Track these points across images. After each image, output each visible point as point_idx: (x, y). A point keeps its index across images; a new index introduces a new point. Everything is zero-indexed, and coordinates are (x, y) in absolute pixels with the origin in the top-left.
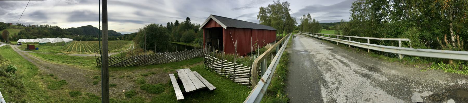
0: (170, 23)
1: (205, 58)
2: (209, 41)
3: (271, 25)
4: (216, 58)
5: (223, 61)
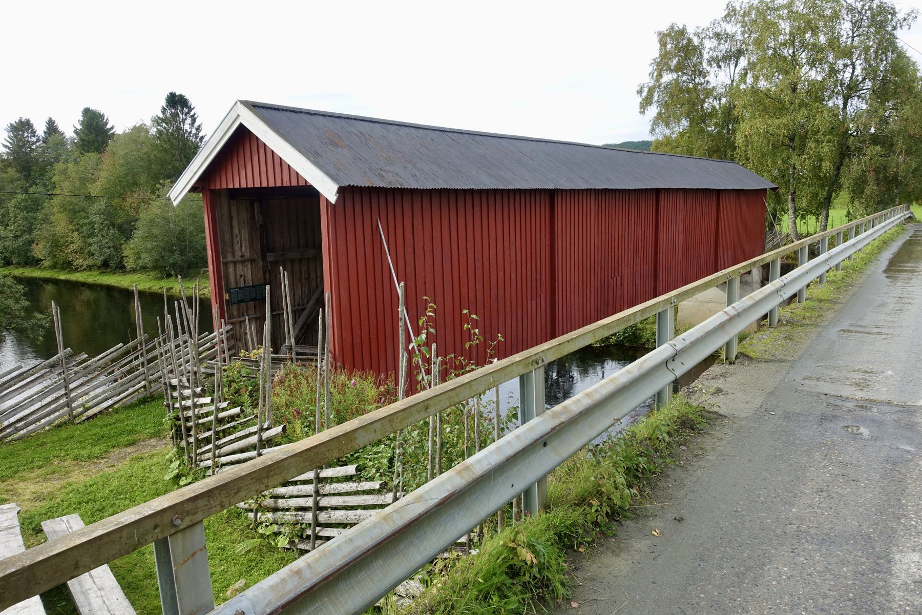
0: (40, 129)
5: (262, 430)
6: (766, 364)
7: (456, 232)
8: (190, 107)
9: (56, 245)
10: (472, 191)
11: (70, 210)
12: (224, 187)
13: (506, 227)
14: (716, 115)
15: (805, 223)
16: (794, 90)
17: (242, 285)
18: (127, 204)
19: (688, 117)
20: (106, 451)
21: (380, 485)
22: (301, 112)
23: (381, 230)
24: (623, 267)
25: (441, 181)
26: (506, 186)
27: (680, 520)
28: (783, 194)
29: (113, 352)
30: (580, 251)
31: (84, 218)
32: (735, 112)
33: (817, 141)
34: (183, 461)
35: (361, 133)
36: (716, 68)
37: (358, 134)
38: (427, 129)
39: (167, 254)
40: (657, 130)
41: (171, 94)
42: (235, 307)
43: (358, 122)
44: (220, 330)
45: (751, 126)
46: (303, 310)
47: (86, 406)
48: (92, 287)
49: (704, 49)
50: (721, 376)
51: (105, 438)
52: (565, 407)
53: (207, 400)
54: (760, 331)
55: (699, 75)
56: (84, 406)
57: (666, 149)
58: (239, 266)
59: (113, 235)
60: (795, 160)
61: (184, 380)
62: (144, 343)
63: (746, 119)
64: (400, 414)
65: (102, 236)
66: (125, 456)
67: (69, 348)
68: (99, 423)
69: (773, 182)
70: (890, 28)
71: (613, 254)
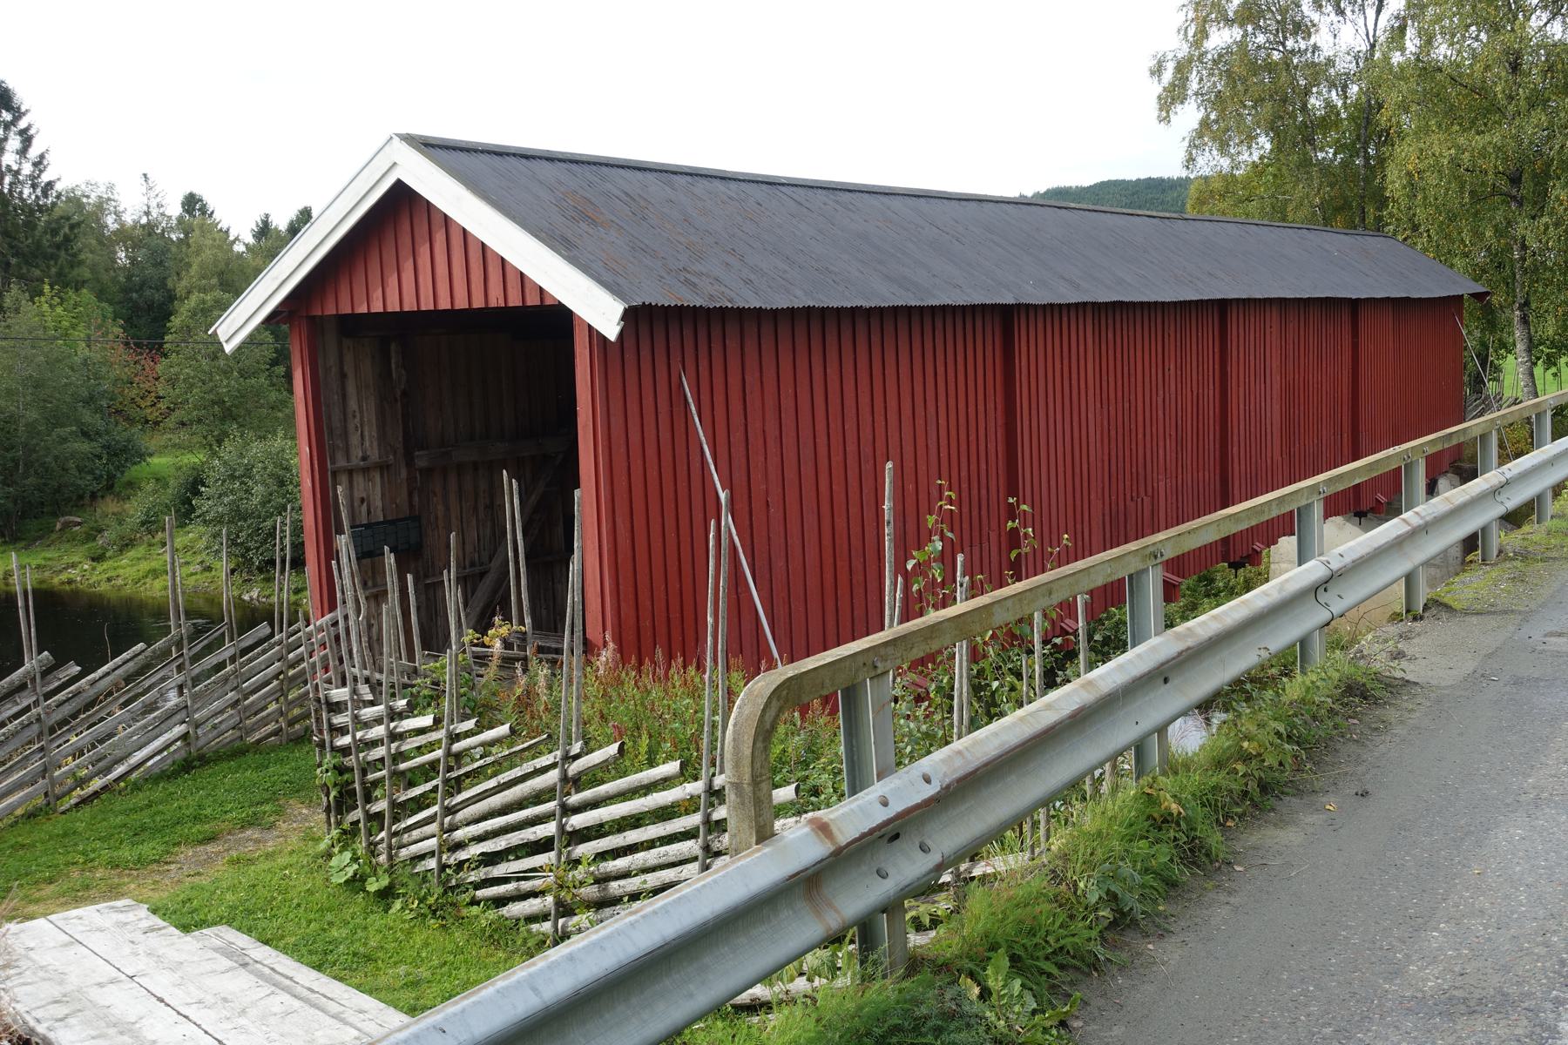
1: (345, 740)
3: (1382, 202)
4: (480, 728)
5: (569, 758)
6: (1479, 617)
8: (19, 108)
13: (918, 388)
14: (1339, 121)
15: (1555, 375)
16: (1515, 67)
17: (365, 522)
19: (1272, 129)
24: (1155, 475)
25: (799, 293)
26: (922, 300)
27: (1365, 794)
28: (1501, 307)
32: (1383, 119)
35: (627, 194)
36: (1333, 15)
38: (744, 181)
45: (1421, 150)
46: (482, 575)
50: (1401, 637)
52: (1189, 629)
53: (427, 721)
54: (1464, 571)
55: (1295, 33)
56: (74, 774)
57: (1222, 206)
58: (359, 480)
60: (1523, 228)
62: (185, 642)
63: (1408, 135)
64: (1028, 594)
67: (46, 653)
69: (1476, 279)
71: (1134, 447)
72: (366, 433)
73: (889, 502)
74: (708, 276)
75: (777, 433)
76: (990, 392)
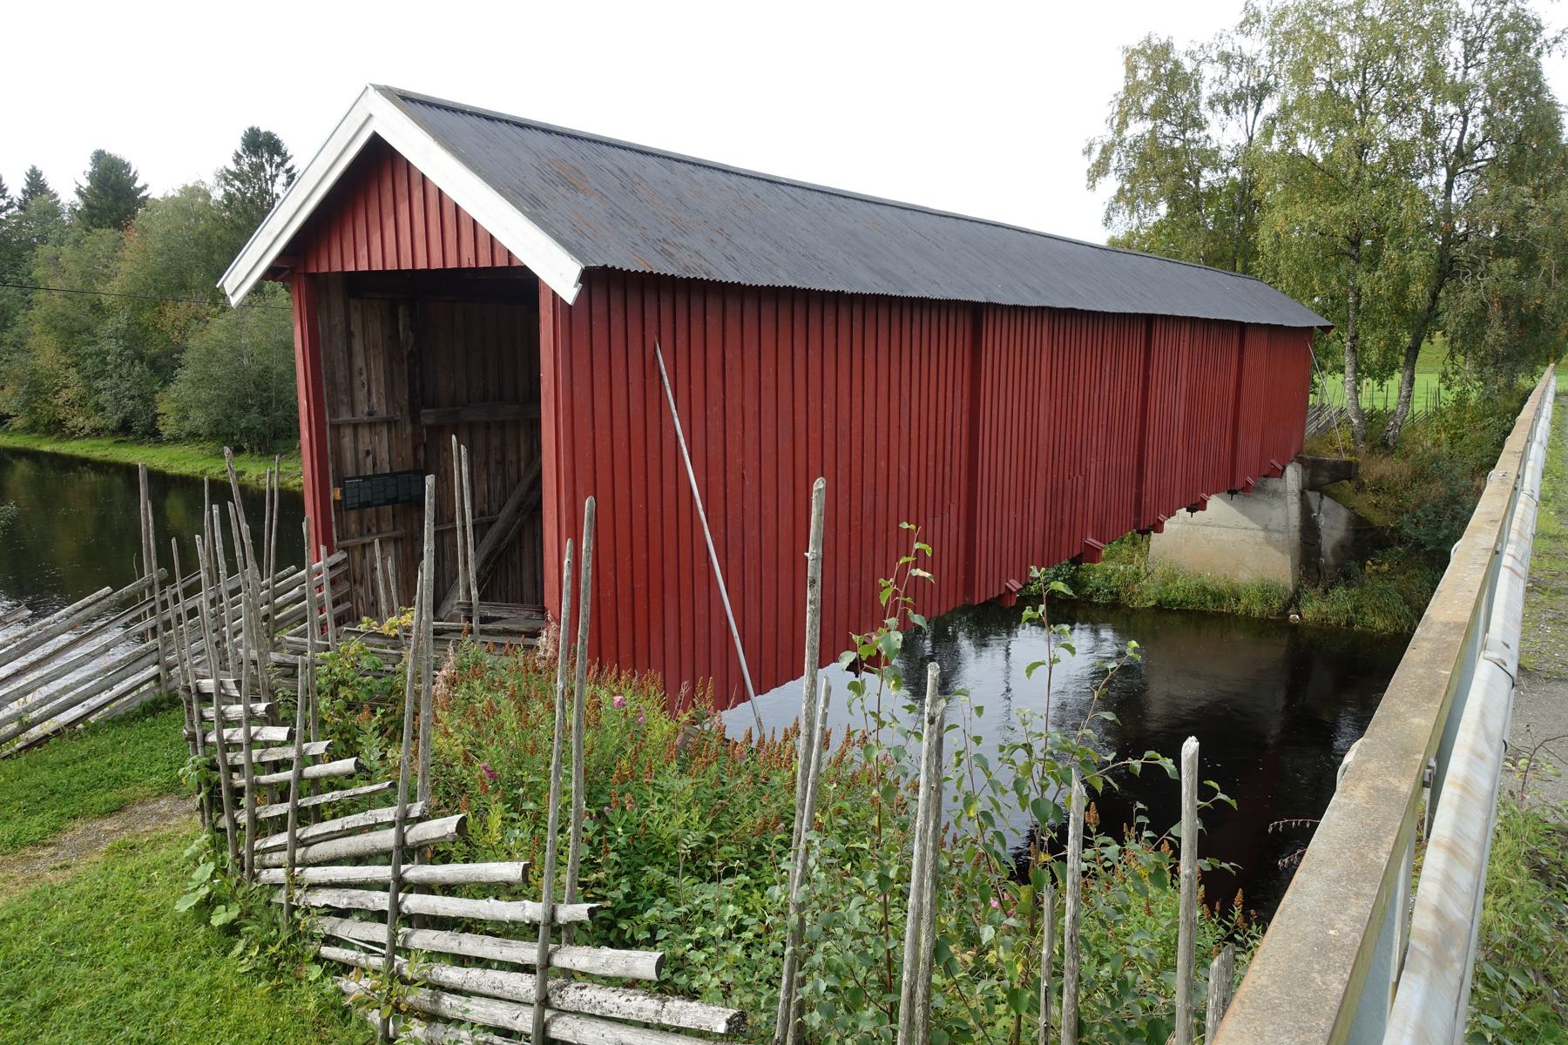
2: (384, 455)
5: (406, 820)
7: (803, 378)
9: (37, 389)
10: (838, 295)
11: (63, 329)
12: (337, 268)
17: (370, 473)
18: (167, 322)
20: (54, 829)
21: (729, 1022)
22: (500, 120)
23: (663, 367)
25: (782, 273)
29: (89, 605)
30: (1022, 426)
31: (89, 344)
33: (1400, 247)
34: (223, 864)
35: (621, 170)
37: (617, 172)
38: (746, 176)
39: (236, 412)
40: (1116, 220)
41: (252, 129)
42: (353, 515)
43: (612, 150)
44: (320, 563)
46: (491, 524)
47: (26, 719)
48: (101, 467)
49: (1201, 80)
51: (57, 795)
53: (280, 733)
56: (20, 718)
58: (364, 434)
59: (139, 376)
60: (1363, 280)
61: (230, 682)
62: (157, 587)
65: (121, 376)
66: (97, 840)
68: (52, 758)
70: (1531, 54)
72: (374, 390)
73: (816, 547)
74: (688, 249)
75: (757, 408)
76: (958, 380)
